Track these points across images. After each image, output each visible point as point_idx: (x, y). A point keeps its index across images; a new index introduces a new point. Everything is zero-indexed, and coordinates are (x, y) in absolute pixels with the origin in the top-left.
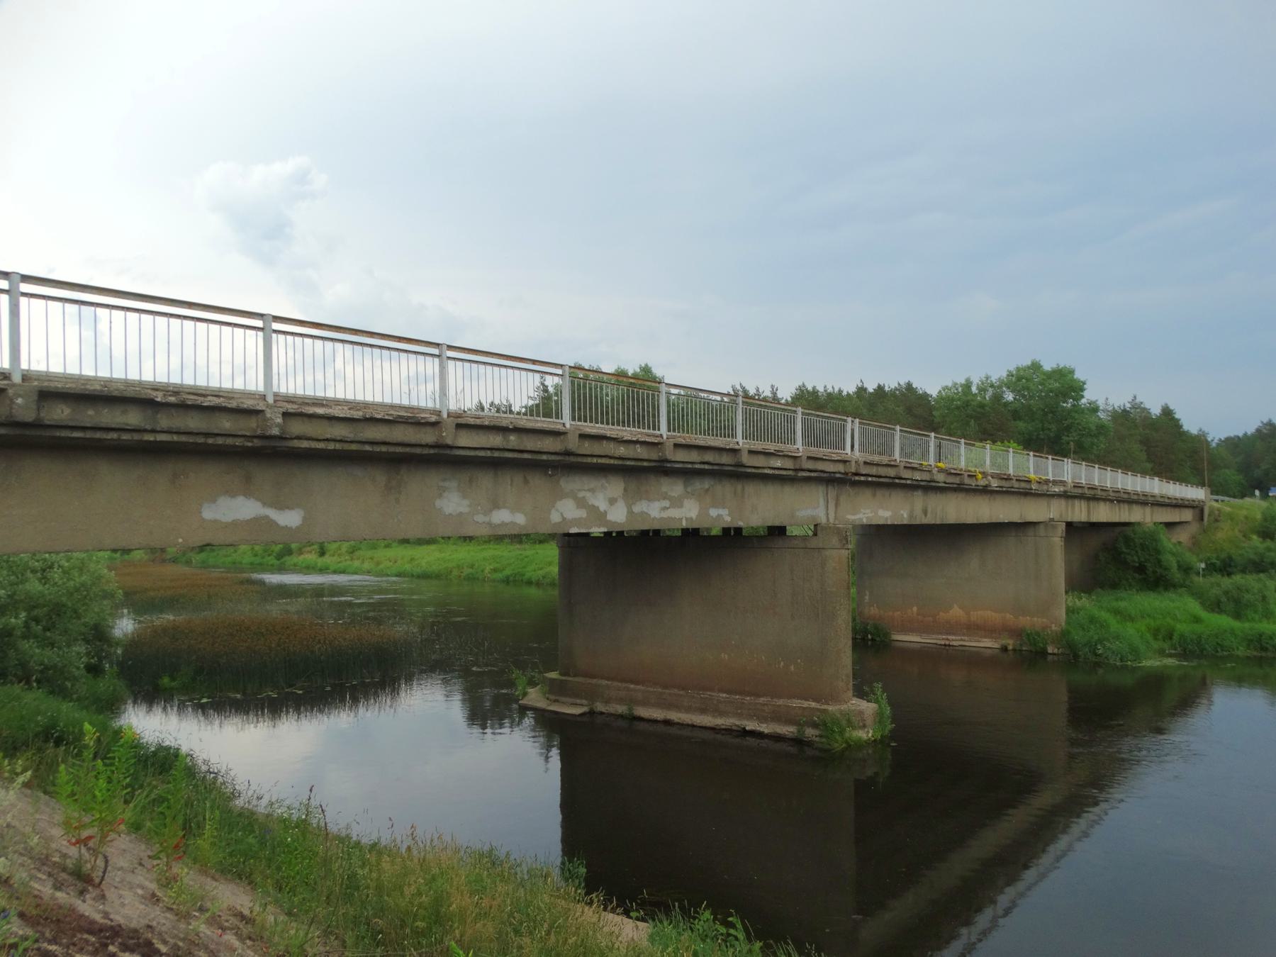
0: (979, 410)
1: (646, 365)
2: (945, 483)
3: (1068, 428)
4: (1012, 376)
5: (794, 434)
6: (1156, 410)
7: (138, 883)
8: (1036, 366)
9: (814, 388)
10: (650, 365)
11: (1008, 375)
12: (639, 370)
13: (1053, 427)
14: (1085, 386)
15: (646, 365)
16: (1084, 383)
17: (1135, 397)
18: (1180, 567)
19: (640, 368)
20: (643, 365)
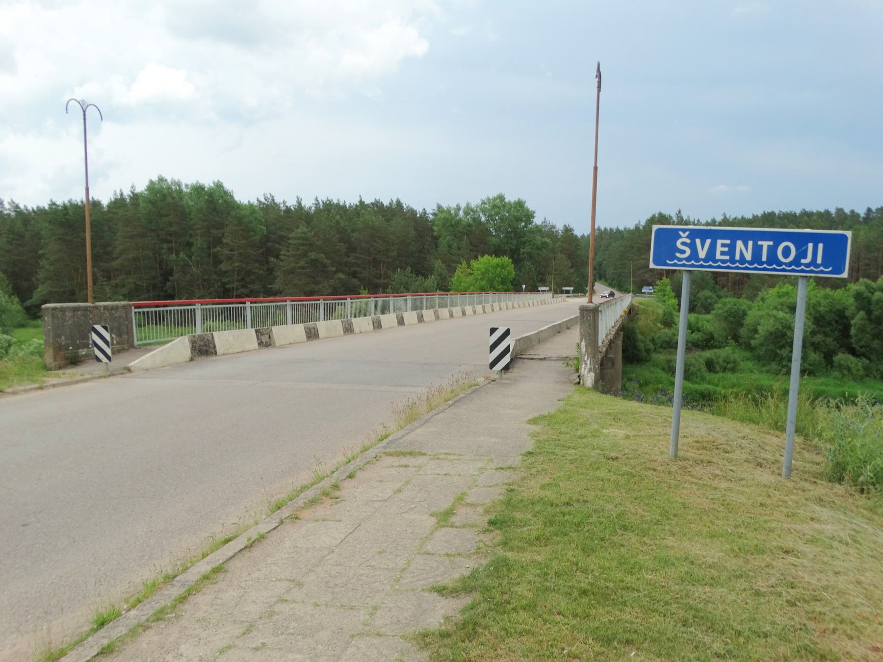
0: (467, 228)
1: (218, 181)
2: (119, 620)
3: (524, 243)
4: (485, 203)
5: (204, 314)
6: (560, 227)
7: (765, 557)
8: (501, 198)
9: (249, 202)
10: (221, 181)
11: (482, 203)
12: (213, 186)
13: (515, 242)
14: (535, 215)
15: (218, 181)
16: (534, 212)
17: (545, 219)
18: (645, 350)
19: (214, 184)
20: (216, 181)
